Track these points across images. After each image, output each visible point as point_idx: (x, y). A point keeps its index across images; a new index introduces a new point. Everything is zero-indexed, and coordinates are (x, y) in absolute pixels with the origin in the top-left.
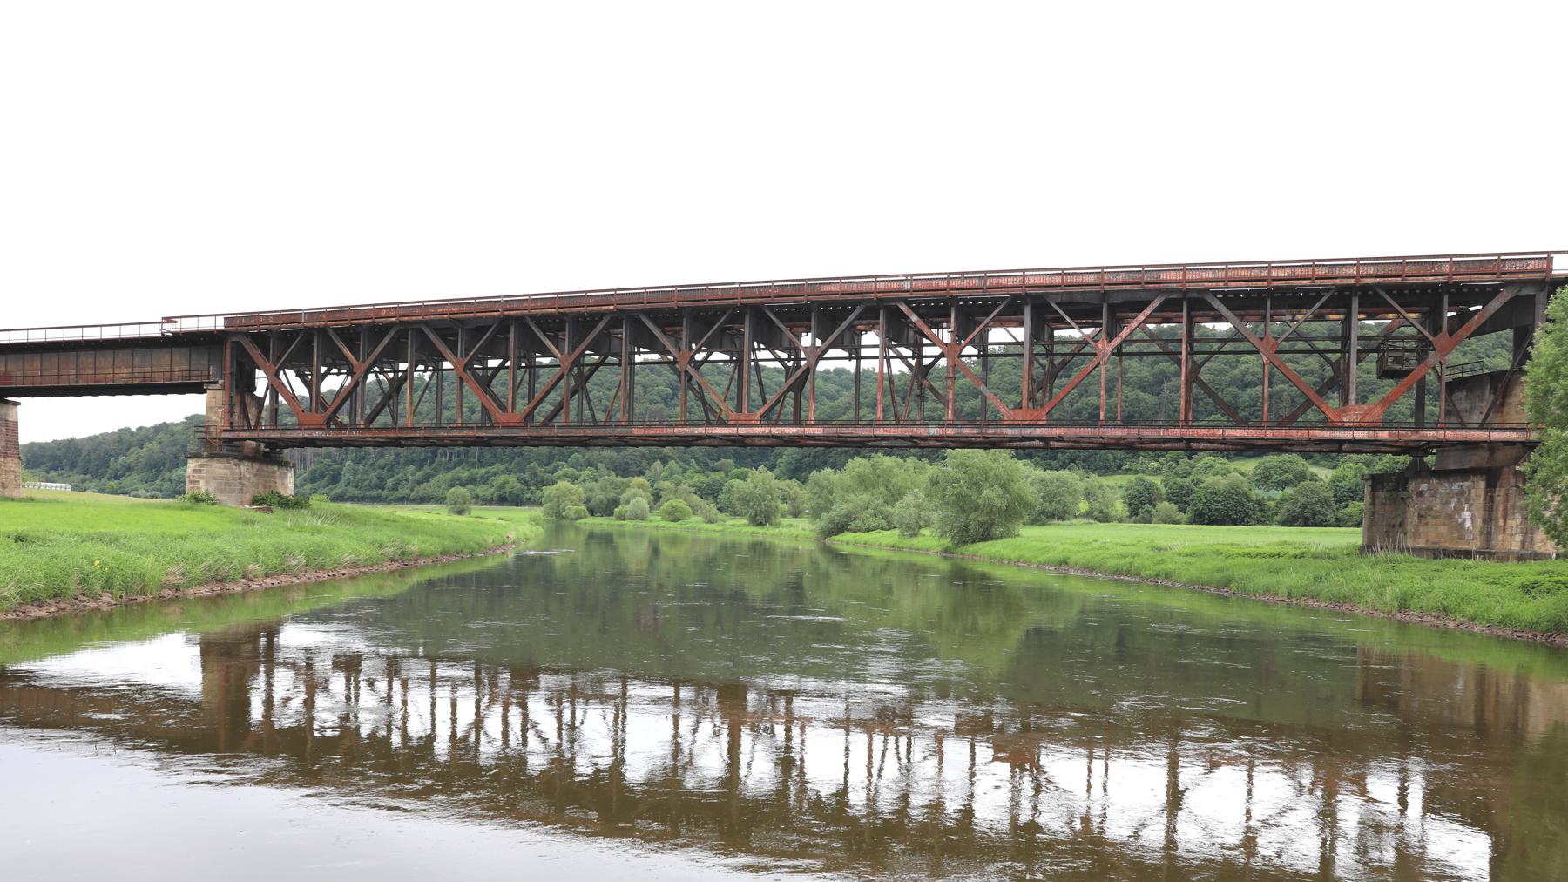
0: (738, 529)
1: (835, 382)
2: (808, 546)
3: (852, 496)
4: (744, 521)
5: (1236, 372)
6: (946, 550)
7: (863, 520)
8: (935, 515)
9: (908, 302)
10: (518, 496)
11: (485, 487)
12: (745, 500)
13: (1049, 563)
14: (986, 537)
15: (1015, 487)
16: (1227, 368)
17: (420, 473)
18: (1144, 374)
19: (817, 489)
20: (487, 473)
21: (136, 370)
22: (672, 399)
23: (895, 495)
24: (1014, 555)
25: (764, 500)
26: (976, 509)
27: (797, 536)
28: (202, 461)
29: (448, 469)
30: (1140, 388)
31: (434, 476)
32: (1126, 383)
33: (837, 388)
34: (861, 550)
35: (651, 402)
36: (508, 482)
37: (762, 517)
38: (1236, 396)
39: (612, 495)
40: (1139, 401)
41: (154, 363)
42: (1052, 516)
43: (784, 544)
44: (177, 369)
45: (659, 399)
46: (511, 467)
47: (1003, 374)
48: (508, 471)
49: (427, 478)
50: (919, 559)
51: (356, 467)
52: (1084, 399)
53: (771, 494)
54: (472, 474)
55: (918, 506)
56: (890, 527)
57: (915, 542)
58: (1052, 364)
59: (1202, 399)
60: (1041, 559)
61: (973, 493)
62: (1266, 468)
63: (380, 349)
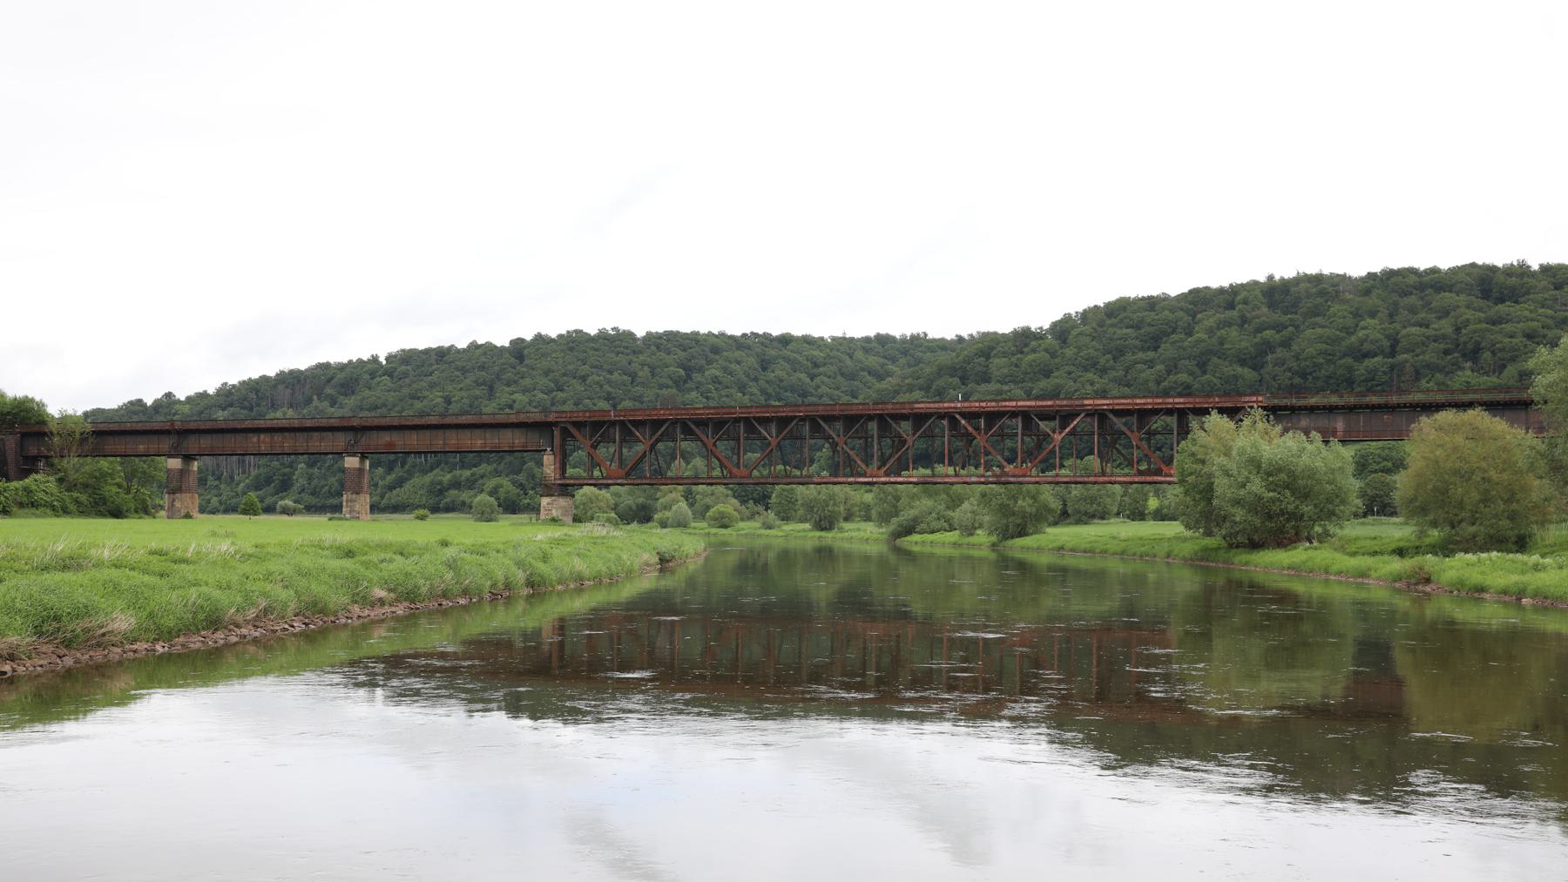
0: (798, 534)
1: (877, 354)
2: (874, 549)
3: (918, 503)
4: (807, 526)
5: (1353, 339)
6: (994, 545)
7: (928, 523)
8: (987, 518)
9: (960, 413)
10: (514, 502)
11: (472, 493)
12: (810, 506)
13: (1053, 549)
14: (1022, 533)
15: (1042, 498)
16: (1343, 334)
17: (390, 478)
18: (1244, 344)
19: (882, 495)
20: (472, 475)
21: (487, 442)
22: (685, 382)
23: (955, 502)
24: (1035, 546)
25: (827, 506)
26: (1014, 514)
27: (867, 539)
28: (554, 498)
29: (424, 472)
30: (1239, 361)
31: (408, 479)
32: (1223, 356)
33: (882, 360)
34: (928, 549)
35: (661, 386)
36: (502, 486)
37: (825, 523)
38: (1350, 369)
39: (641, 500)
40: (1236, 377)
41: (501, 437)
42: (1093, 516)
43: (856, 547)
44: (517, 441)
45: (670, 383)
46: (500, 468)
47: (1079, 348)
48: (497, 473)
49: (400, 483)
50: (976, 553)
51: (310, 471)
52: (1172, 378)
53: (835, 500)
54: (455, 476)
55: (973, 512)
56: (952, 529)
57: (972, 540)
58: (1038, 439)
59: (1311, 374)
60: (1050, 547)
61: (1011, 503)
62: (1362, 456)
63: (660, 433)
